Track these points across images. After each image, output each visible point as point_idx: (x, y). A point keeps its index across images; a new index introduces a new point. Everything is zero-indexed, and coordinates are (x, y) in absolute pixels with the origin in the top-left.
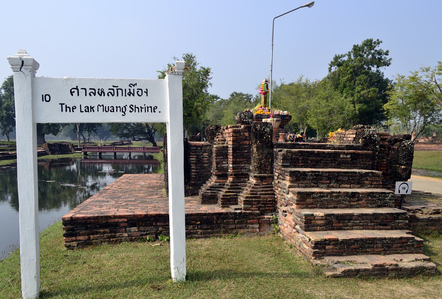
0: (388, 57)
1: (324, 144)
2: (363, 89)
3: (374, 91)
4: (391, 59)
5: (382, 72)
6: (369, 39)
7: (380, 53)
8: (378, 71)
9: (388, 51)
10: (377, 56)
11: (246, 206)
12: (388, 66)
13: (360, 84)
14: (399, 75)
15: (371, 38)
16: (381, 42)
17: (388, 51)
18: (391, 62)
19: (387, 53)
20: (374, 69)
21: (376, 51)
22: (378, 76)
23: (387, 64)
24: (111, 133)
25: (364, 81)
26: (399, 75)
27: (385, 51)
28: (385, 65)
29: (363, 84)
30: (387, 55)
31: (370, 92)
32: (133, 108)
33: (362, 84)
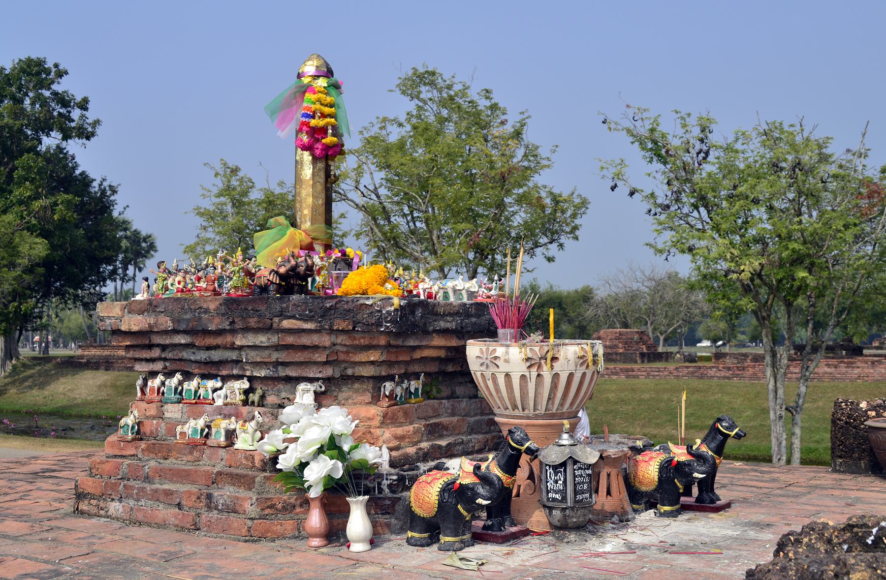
0: (91, 116)
2: (37, 197)
4: (97, 123)
5: (71, 153)
7: (63, 100)
8: (60, 149)
9: (86, 101)
10: (59, 109)
11: (611, 366)
12: (88, 138)
14: (225, 164)
15: (41, 56)
17: (86, 101)
19: (84, 105)
21: (55, 94)
22: (59, 157)
23: (85, 134)
25: (39, 173)
26: (225, 164)
27: (79, 99)
28: (80, 136)
29: (34, 179)
30: (86, 109)
31: (56, 204)
32: (285, 364)
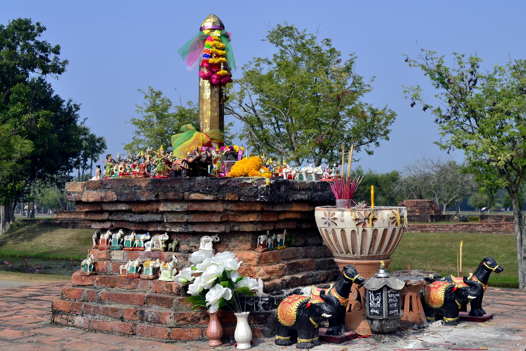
0: (62, 58)
1: (372, 200)
2: (25, 112)
3: (46, 116)
6: (23, 18)
7: (43, 47)
9: (58, 47)
10: (40, 54)
12: (60, 73)
13: (19, 101)
14: (152, 90)
15: (28, 18)
16: (45, 29)
17: (58, 47)
18: (67, 67)
19: (57, 50)
20: (34, 75)
21: (38, 43)
22: (41, 87)
23: (58, 70)
24: (293, 204)
25: (27, 96)
26: (152, 90)
27: (53, 46)
29: (23, 100)
31: (38, 117)
33: (22, 102)
